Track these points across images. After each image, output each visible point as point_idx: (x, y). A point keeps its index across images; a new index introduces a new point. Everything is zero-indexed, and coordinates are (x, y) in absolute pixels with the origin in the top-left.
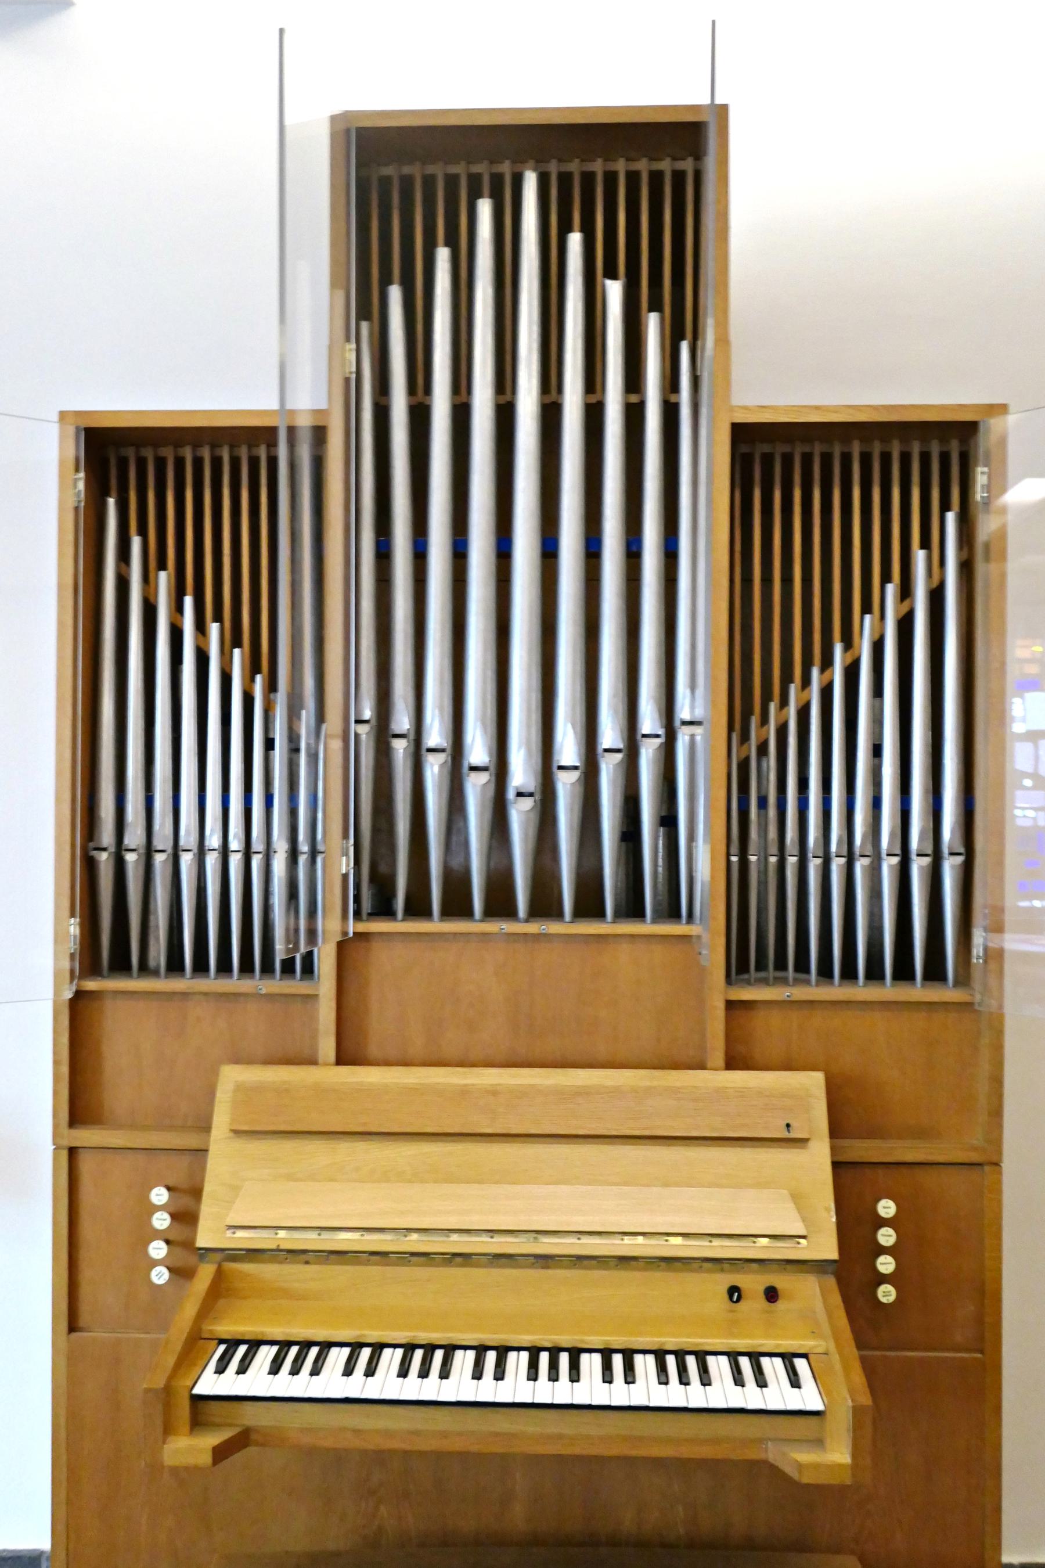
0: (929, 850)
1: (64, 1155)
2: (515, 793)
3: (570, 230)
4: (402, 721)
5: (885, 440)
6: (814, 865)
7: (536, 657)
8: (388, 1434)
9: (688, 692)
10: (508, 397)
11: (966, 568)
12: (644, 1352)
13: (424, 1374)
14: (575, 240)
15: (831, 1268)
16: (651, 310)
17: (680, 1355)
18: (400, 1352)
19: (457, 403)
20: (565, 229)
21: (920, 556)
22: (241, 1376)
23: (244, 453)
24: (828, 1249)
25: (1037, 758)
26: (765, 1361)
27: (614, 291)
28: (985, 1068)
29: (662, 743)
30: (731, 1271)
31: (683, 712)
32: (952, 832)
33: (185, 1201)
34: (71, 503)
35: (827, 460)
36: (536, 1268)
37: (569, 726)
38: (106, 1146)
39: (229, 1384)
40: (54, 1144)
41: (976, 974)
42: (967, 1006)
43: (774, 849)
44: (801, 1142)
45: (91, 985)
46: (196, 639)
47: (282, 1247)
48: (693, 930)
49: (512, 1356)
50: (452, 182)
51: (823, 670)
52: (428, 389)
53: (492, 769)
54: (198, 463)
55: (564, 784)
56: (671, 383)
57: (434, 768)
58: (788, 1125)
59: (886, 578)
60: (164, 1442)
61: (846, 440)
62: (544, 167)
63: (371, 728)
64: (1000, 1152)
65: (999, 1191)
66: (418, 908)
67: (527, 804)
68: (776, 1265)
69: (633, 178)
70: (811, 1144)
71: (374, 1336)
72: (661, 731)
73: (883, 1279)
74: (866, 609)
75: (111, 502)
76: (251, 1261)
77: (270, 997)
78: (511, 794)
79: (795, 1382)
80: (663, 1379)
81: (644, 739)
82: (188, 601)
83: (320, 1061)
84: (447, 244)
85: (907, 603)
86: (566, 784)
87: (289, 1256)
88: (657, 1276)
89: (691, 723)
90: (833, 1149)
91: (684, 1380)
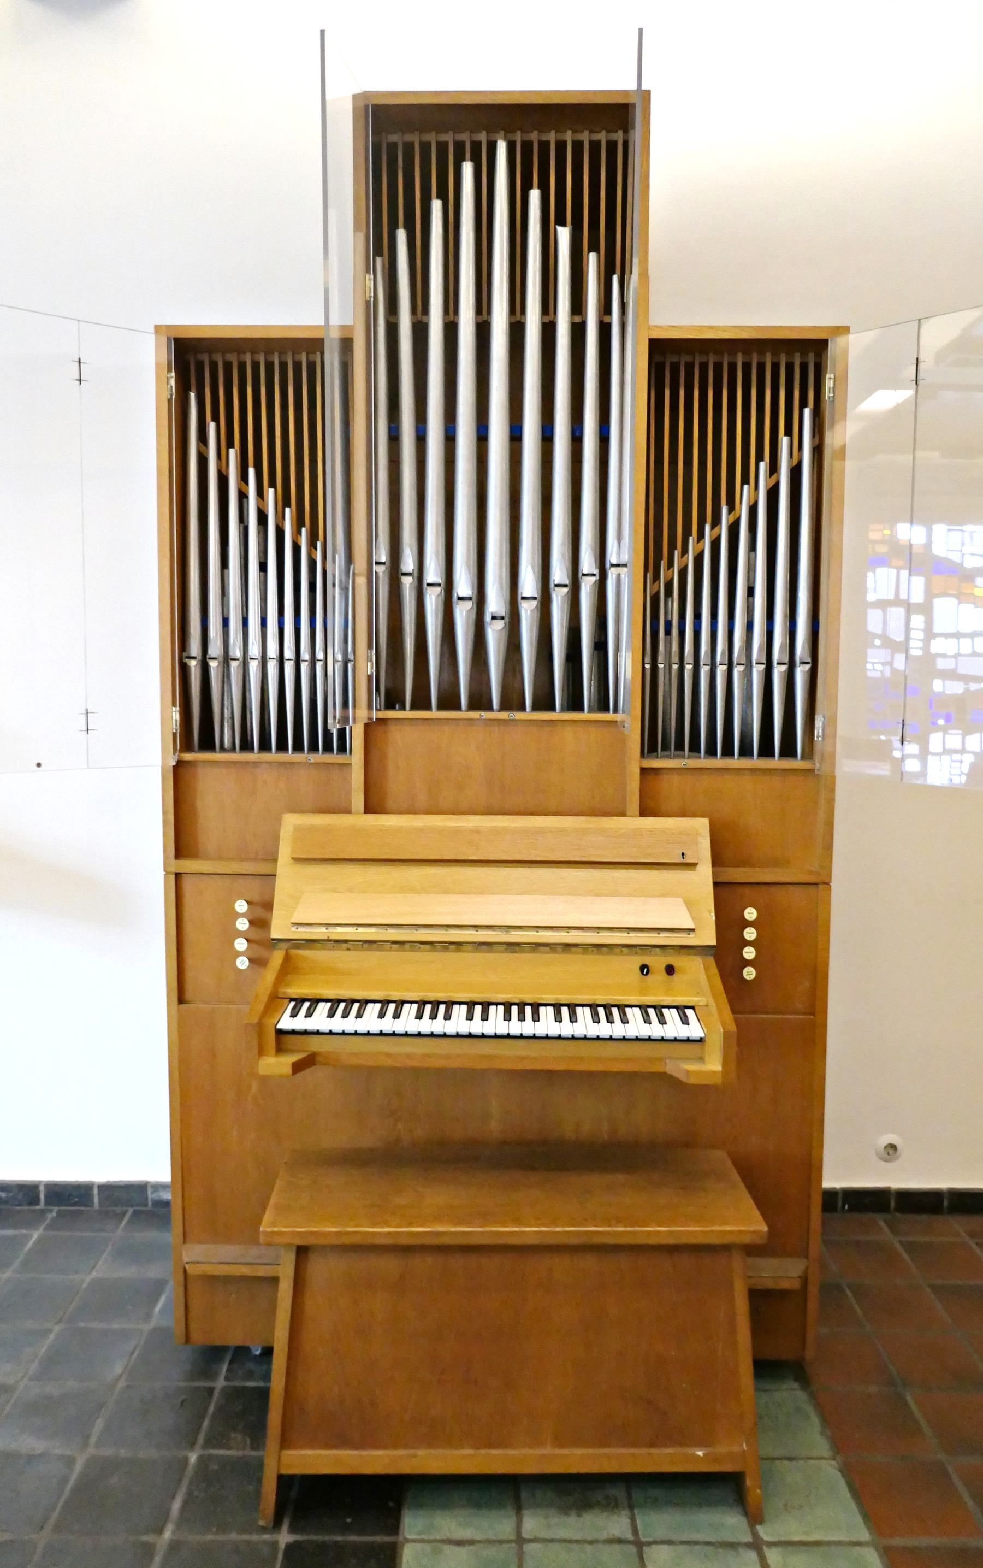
0: (786, 660)
1: (173, 877)
2: (491, 617)
3: (531, 187)
4: (408, 563)
5: (762, 353)
6: (704, 671)
7: (506, 517)
8: (409, 1056)
9: (616, 544)
10: (551, 317)
11: (818, 451)
12: (583, 1006)
13: (433, 1016)
14: (535, 195)
15: (712, 951)
16: (589, 251)
17: (607, 1007)
18: (415, 1006)
19: (480, 321)
20: (527, 187)
21: (784, 441)
22: (308, 1018)
23: (262, 359)
24: (708, 937)
25: (885, 622)
26: (665, 1011)
27: (564, 235)
28: (821, 815)
29: (596, 581)
30: (642, 954)
31: (612, 557)
32: (803, 647)
33: (260, 912)
34: (165, 396)
35: (718, 367)
36: (507, 953)
37: (530, 567)
38: (201, 872)
39: (300, 1023)
40: (165, 871)
41: (818, 747)
42: (811, 771)
43: (675, 659)
44: (692, 866)
45: (188, 756)
46: (257, 502)
47: (330, 938)
48: (619, 717)
49: (492, 1008)
50: (442, 147)
51: (712, 528)
52: (426, 310)
53: (474, 599)
54: (256, 366)
55: (526, 610)
56: (605, 308)
57: (433, 600)
58: (683, 854)
59: (760, 458)
60: (259, 1060)
61: (733, 353)
62: (511, 137)
63: (386, 568)
64: (829, 875)
65: (828, 903)
66: (421, 702)
67: (500, 625)
68: (673, 950)
69: (578, 146)
70: (698, 867)
71: (396, 996)
72: (596, 571)
73: (748, 963)
74: (745, 481)
75: (193, 395)
76: (311, 949)
77: (317, 765)
78: (488, 618)
79: (685, 1021)
80: (596, 1019)
81: (584, 578)
82: (251, 472)
83: (353, 810)
84: (438, 197)
85: (774, 477)
86: (528, 611)
87: (335, 945)
88: (591, 958)
89: (618, 565)
90: (715, 874)
91: (610, 1019)
